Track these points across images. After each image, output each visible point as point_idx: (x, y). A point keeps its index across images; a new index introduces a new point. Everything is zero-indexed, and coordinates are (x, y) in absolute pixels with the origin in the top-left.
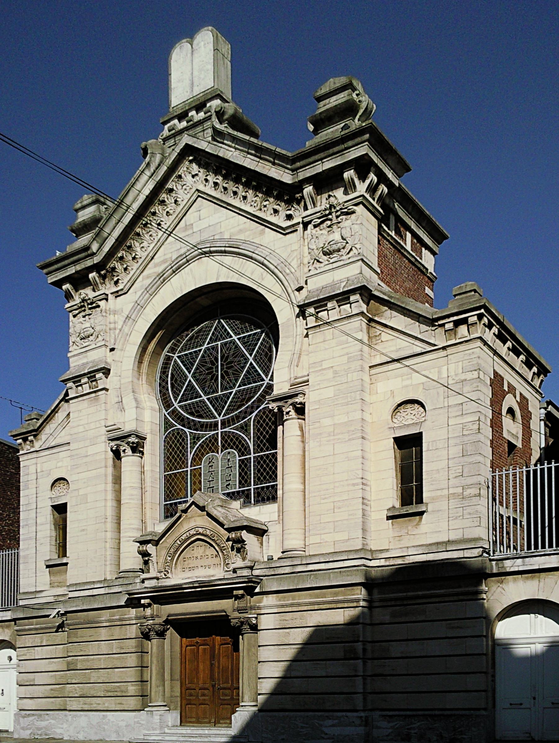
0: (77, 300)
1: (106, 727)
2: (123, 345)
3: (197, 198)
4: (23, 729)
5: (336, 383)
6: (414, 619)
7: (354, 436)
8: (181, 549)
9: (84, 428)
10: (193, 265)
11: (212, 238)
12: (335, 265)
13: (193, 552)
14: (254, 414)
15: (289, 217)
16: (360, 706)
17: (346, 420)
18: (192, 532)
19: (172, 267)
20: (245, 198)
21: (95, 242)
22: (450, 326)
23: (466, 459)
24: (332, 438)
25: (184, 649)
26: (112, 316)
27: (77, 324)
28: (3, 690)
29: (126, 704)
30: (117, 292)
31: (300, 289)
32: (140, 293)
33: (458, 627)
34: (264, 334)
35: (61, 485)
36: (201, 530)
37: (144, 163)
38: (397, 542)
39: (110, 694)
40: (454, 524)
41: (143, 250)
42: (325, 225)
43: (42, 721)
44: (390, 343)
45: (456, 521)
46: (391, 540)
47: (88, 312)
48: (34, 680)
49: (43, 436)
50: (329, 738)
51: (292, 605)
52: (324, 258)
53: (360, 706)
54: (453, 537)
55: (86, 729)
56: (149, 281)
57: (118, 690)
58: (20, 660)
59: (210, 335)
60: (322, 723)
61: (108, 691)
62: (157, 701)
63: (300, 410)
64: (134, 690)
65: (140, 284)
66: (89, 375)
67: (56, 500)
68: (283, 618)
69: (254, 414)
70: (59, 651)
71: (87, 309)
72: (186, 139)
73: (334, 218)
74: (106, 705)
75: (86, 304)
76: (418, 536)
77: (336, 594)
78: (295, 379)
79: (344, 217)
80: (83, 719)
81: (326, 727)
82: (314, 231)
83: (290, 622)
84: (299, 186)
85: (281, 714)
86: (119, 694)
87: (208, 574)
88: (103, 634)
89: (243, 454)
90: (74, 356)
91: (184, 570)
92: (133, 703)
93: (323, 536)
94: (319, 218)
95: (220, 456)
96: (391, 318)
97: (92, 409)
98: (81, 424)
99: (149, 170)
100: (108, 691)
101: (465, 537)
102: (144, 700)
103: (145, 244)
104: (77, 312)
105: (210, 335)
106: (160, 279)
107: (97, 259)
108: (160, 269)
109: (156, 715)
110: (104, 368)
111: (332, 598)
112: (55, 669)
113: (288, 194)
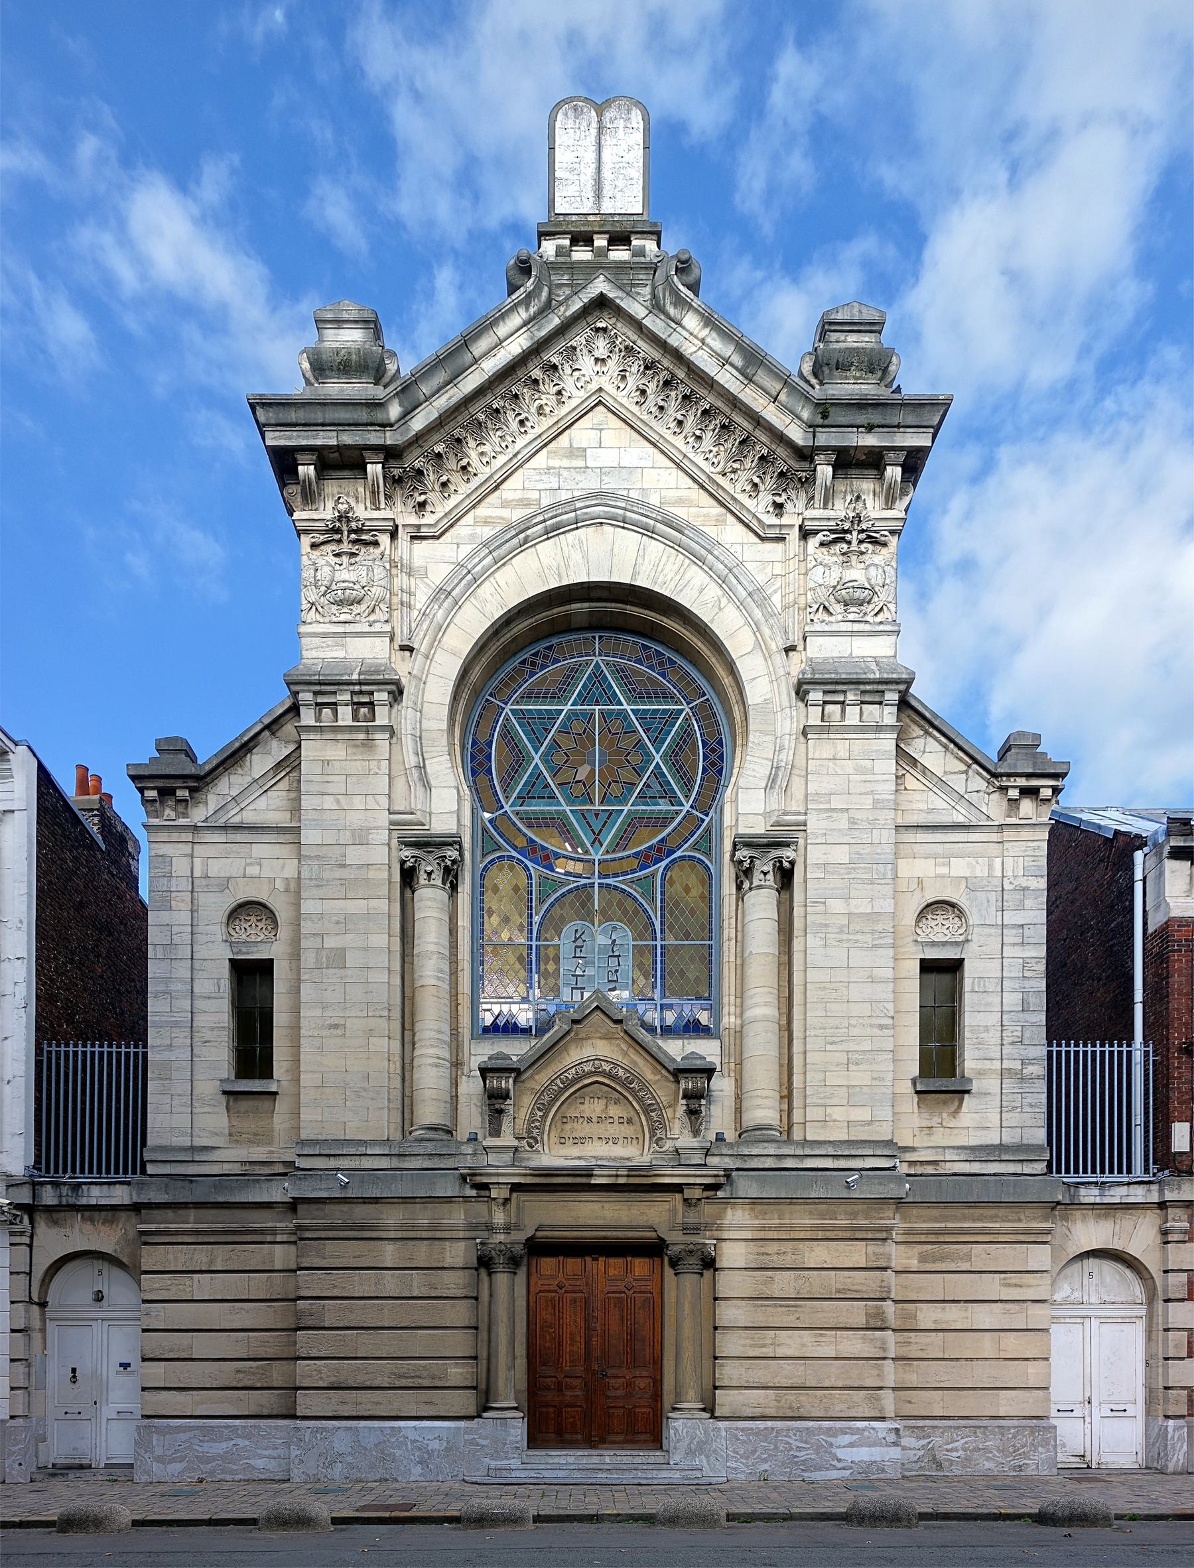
0: (326, 512)
1: (398, 1453)
3: (595, 406)
4: (160, 1459)
5: (853, 841)
6: (953, 1267)
7: (881, 941)
8: (563, 1098)
9: (338, 802)
12: (857, 627)
13: (582, 1107)
14: (663, 864)
16: (890, 1411)
18: (588, 1068)
19: (545, 521)
21: (396, 401)
22: (1014, 793)
24: (845, 937)
25: (532, 1299)
26: (405, 577)
28: (74, 1370)
33: (1016, 1285)
35: (253, 919)
36: (606, 1067)
38: (926, 1137)
39: (404, 1383)
40: (1012, 1119)
44: (917, 796)
45: (1011, 1114)
49: (213, 800)
50: (844, 1468)
51: (778, 1229)
52: (837, 608)
54: (1007, 1139)
55: (350, 1459)
56: (488, 532)
57: (425, 1374)
58: (145, 1301)
61: (400, 1376)
62: (506, 1399)
63: (785, 876)
64: (461, 1374)
66: (357, 688)
68: (763, 1250)
73: (855, 542)
76: (956, 1131)
77: (854, 1215)
78: (784, 814)
79: (870, 546)
80: (341, 1436)
81: (839, 1447)
83: (775, 1257)
84: (806, 455)
85: (760, 1424)
86: (426, 1383)
87: (613, 1155)
88: (389, 1254)
92: (465, 1402)
93: (829, 1110)
94: (832, 532)
96: (924, 752)
98: (329, 791)
99: (527, 309)
100: (400, 1376)
101: (1025, 1142)
103: (486, 448)
106: (517, 535)
107: (390, 438)
108: (518, 514)
111: (943, 1225)
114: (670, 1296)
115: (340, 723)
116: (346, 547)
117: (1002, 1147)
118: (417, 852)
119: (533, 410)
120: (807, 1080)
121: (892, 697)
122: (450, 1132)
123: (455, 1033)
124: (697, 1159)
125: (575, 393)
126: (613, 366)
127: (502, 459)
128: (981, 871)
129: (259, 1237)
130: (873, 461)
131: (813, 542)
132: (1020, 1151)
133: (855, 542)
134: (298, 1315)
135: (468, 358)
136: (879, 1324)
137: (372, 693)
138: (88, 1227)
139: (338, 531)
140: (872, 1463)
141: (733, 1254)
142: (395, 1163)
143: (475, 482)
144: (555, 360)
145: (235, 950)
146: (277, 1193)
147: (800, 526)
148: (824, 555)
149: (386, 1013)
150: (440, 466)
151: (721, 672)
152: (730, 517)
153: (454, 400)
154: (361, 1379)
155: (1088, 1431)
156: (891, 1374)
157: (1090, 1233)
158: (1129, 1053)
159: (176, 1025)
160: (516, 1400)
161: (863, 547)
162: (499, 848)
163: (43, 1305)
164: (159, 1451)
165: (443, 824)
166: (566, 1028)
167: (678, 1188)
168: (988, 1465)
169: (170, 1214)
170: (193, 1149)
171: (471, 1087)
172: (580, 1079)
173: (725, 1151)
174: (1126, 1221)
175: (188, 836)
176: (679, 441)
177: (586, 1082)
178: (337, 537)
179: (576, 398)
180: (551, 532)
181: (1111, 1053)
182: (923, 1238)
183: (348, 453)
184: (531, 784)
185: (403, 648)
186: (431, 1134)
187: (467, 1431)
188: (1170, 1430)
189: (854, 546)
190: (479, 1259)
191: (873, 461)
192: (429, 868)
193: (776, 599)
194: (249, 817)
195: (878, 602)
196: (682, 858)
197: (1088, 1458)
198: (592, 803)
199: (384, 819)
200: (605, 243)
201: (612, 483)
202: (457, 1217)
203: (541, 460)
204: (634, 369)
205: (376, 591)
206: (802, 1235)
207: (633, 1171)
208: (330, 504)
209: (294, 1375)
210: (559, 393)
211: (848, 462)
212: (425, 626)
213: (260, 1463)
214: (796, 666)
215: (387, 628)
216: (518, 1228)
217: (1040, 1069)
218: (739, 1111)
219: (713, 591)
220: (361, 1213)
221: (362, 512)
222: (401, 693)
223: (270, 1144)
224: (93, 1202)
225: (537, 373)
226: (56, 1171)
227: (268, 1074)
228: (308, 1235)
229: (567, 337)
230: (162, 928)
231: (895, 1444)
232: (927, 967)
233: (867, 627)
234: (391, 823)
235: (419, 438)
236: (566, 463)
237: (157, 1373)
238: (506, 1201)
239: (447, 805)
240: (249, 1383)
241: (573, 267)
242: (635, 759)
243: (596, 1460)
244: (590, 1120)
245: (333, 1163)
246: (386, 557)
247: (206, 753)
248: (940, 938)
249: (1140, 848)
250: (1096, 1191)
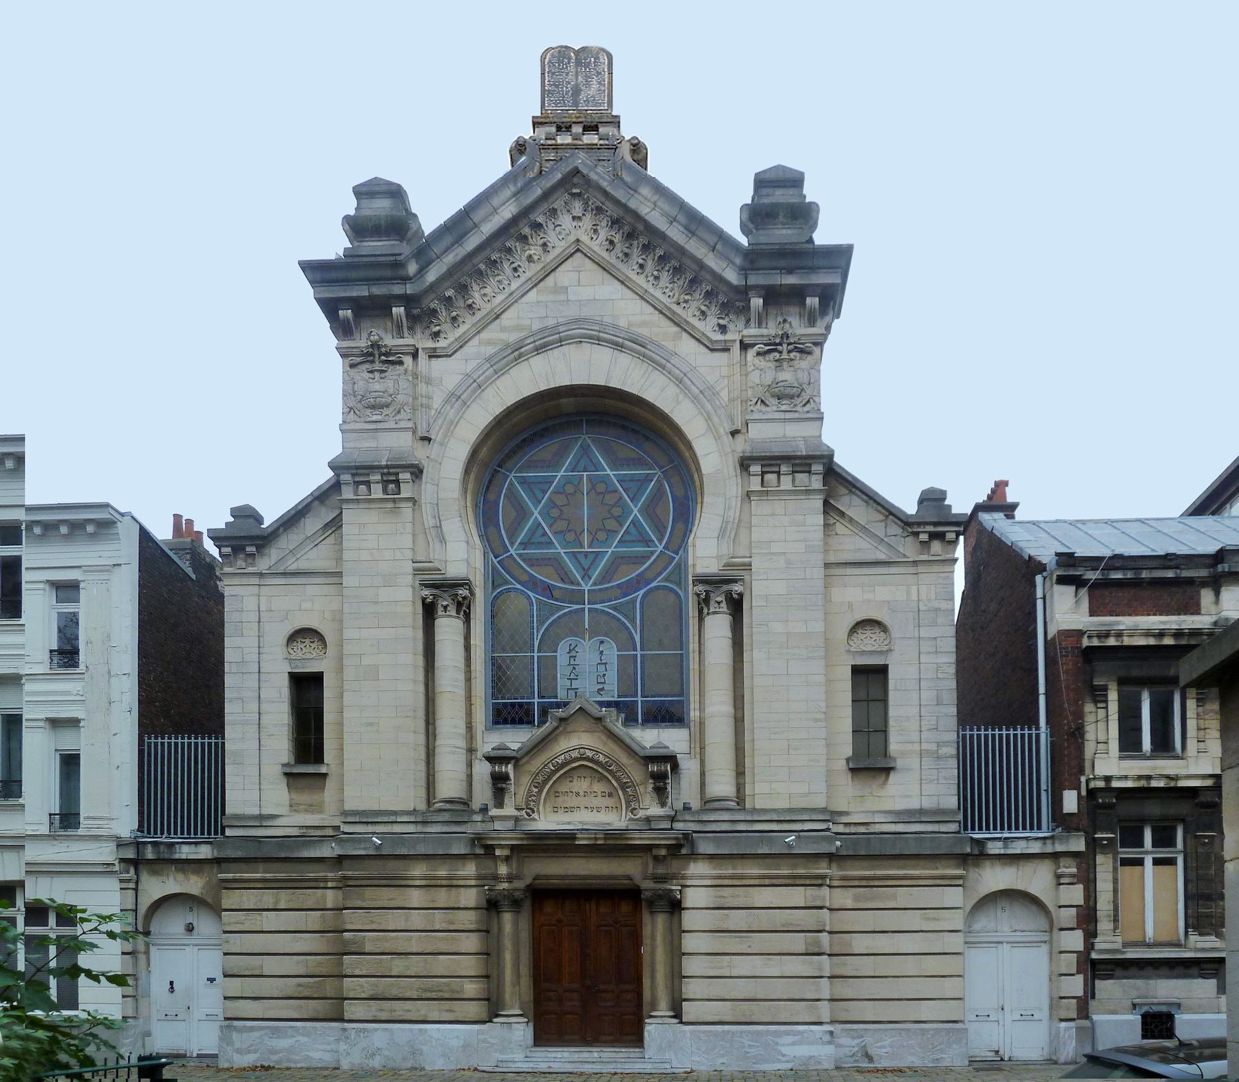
2: (445, 436)
4: (239, 1051)
10: (569, 350)
12: (788, 416)
14: (641, 592)
18: (575, 754)
20: (657, 278)
22: (924, 537)
28: (171, 983)
31: (734, 433)
35: (307, 641)
39: (429, 995)
43: (279, 1037)
51: (732, 877)
52: (774, 401)
55: (386, 1053)
56: (491, 350)
58: (225, 932)
60: (776, 1040)
61: (426, 990)
62: (512, 1007)
63: (736, 606)
69: (641, 592)
70: (313, 920)
73: (785, 353)
75: (376, 353)
77: (795, 866)
80: (380, 1036)
84: (743, 292)
86: (447, 995)
88: (416, 897)
92: (475, 1010)
93: (774, 785)
100: (426, 990)
101: (941, 806)
102: (493, 1009)
103: (488, 290)
104: (358, 360)
107: (410, 289)
108: (513, 337)
110: (412, 466)
112: (306, 950)
114: (647, 931)
115: (373, 496)
116: (377, 366)
117: (921, 811)
119: (524, 258)
120: (757, 762)
121: (818, 468)
122: (465, 804)
123: (470, 727)
124: (666, 825)
125: (558, 243)
126: (587, 222)
127: (500, 298)
128: (900, 595)
129: (316, 884)
130: (796, 295)
131: (751, 353)
132: (938, 815)
133: (785, 353)
134: (345, 943)
135: (469, 224)
136: (816, 950)
137: (398, 474)
138: (180, 876)
139: (372, 354)
140: (810, 1057)
141: (694, 897)
142: (420, 828)
143: (479, 315)
144: (540, 219)
146: (327, 851)
147: (741, 341)
148: (761, 362)
149: (411, 714)
150: (452, 306)
151: (682, 447)
152: (685, 335)
153: (459, 258)
154: (395, 992)
155: (1001, 1032)
156: (825, 989)
157: (995, 878)
158: (1038, 736)
160: (521, 1008)
161: (792, 355)
162: (507, 582)
163: (147, 933)
164: (237, 1045)
165: (454, 570)
166: (555, 724)
167: (649, 848)
168: (911, 1059)
169: (244, 866)
170: (261, 817)
171: (483, 770)
173: (688, 818)
174: (1028, 868)
175: (256, 581)
176: (640, 280)
177: (574, 765)
179: (559, 246)
180: (540, 349)
181: (1015, 736)
182: (856, 883)
184: (532, 532)
185: (424, 439)
186: (448, 806)
187: (478, 1032)
188: (1062, 1031)
189: (785, 355)
190: (488, 901)
191: (796, 295)
192: (445, 603)
193: (724, 394)
194: (303, 565)
195: (805, 396)
196: (657, 588)
197: (1001, 1053)
198: (582, 547)
199: (409, 567)
200: (580, 130)
201: (586, 312)
202: (470, 869)
203: (533, 295)
204: (604, 223)
205: (401, 398)
207: (609, 834)
208: (365, 335)
209: (341, 988)
210: (545, 245)
211: (773, 297)
212: (440, 422)
213: (316, 1055)
214: (741, 446)
215: (410, 425)
216: (518, 877)
217: (952, 751)
218: (703, 784)
219: (672, 390)
220: (393, 868)
221: (390, 341)
222: (421, 472)
223: (321, 812)
224: (184, 857)
225: (526, 231)
226: (156, 833)
227: (319, 759)
228: (351, 883)
229: (551, 200)
230: (238, 648)
231: (830, 1043)
232: (857, 671)
233: (796, 415)
234: (415, 570)
235: (432, 287)
236: (552, 297)
237: (235, 986)
238: (507, 859)
239: (462, 555)
240: (307, 994)
241: (556, 147)
242: (617, 511)
243: (586, 1055)
244: (578, 794)
245: (370, 829)
246: (410, 372)
247: (270, 517)
248: (869, 648)
249: (1040, 573)
250: (1000, 844)
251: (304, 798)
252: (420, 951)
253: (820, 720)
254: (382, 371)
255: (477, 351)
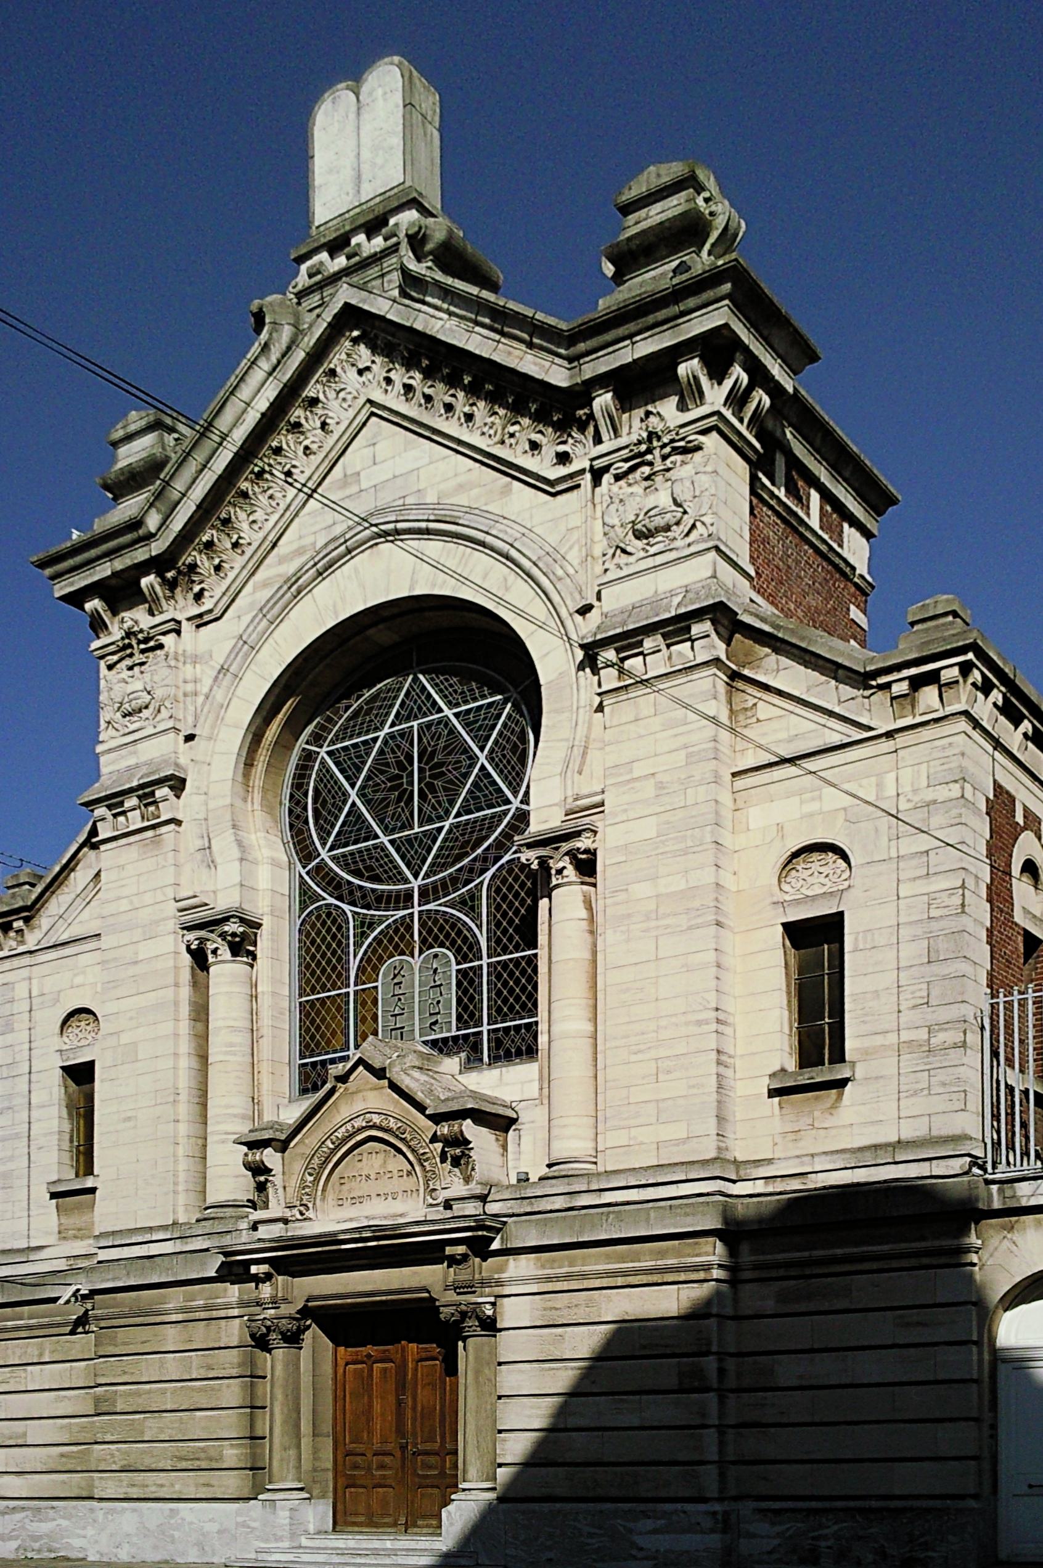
0: (116, 633)
1: (176, 1534)
2: (213, 727)
5: (662, 809)
6: (826, 1306)
8: (335, 1159)
9: (131, 903)
10: (361, 560)
11: (401, 502)
13: (359, 1165)
15: (563, 458)
17: (683, 886)
18: (359, 1123)
19: (315, 564)
20: (469, 417)
21: (153, 511)
23: (936, 968)
24: (653, 924)
26: (189, 667)
27: (116, 684)
29: (220, 1486)
30: (200, 616)
31: (585, 610)
32: (248, 618)
33: (919, 1324)
34: (509, 705)
35: (83, 1024)
37: (257, 344)
40: (912, 1106)
41: (255, 527)
42: (637, 475)
43: (41, 1521)
44: (774, 725)
45: (913, 1100)
46: (778, 1139)
47: (138, 658)
48: (25, 1435)
49: (44, 920)
51: (568, 1277)
53: (712, 1490)
55: (135, 1540)
56: (267, 593)
57: (202, 1455)
59: (397, 706)
60: (630, 1525)
62: (283, 1480)
63: (587, 866)
64: (237, 1455)
65: (249, 599)
66: (141, 792)
67: (72, 1056)
68: (550, 1304)
70: (78, 1373)
71: (136, 651)
72: (345, 294)
73: (658, 460)
74: (177, 1487)
75: (134, 642)
76: (833, 1132)
78: (576, 799)
79: (678, 458)
80: (128, 1517)
81: (641, 1534)
82: (615, 488)
84: (583, 394)
86: (204, 1465)
88: (171, 1337)
89: (465, 959)
90: (110, 751)
91: (340, 1202)
92: (232, 1483)
94: (626, 460)
95: (417, 961)
96: (778, 670)
97: (150, 864)
99: (268, 359)
101: (934, 1133)
102: (258, 1477)
103: (259, 515)
104: (115, 658)
105: (397, 706)
106: (289, 588)
107: (157, 548)
108: (291, 568)
109: (283, 1509)
110: (171, 777)
113: (562, 410)
118: (202, 933)
145: (65, 1058)
154: (148, 1462)
159: (17, 1136)
172: (351, 1136)
177: (359, 1138)
178: (128, 651)
183: (126, 575)
206: (597, 1283)
232: (801, 934)
233: (673, 555)
238: (268, 1277)
248: (820, 890)
251: (74, 1221)
252: (174, 1407)
253: (707, 1022)
254: (142, 664)
255: (252, 597)
